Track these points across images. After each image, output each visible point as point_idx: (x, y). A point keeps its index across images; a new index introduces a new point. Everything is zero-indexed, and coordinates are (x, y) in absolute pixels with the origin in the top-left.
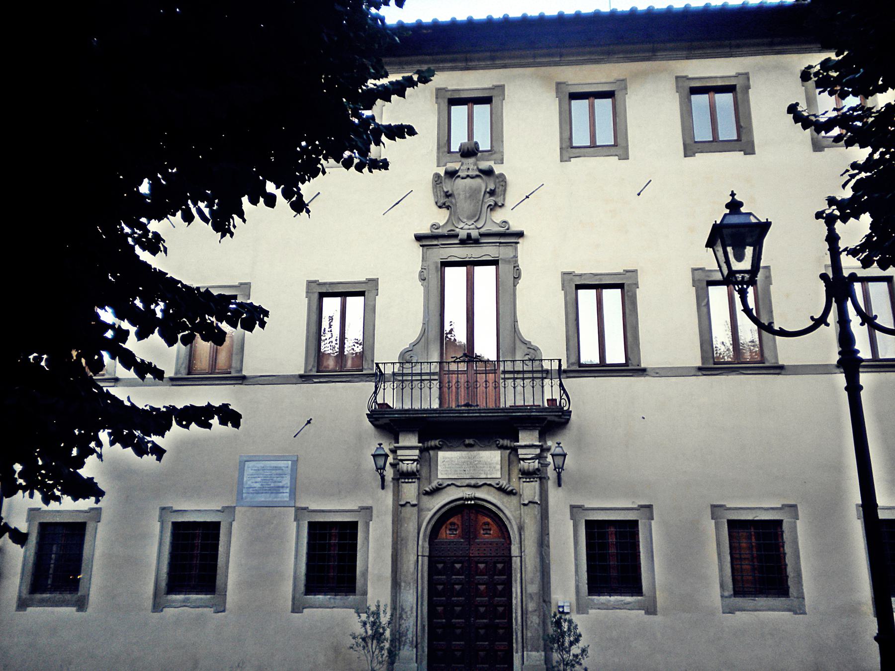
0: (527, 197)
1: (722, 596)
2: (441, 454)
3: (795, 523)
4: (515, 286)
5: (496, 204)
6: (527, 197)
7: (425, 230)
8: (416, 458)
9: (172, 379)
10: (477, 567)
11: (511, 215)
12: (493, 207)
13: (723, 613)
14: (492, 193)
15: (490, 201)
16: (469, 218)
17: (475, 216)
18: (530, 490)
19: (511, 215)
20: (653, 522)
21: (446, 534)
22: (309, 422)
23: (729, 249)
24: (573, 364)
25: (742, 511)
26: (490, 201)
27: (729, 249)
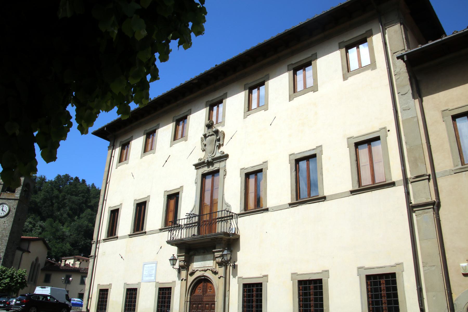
4: (224, 179)
5: (220, 144)
7: (197, 162)
9: (104, 240)
10: (205, 306)
11: (225, 149)
12: (219, 147)
15: (217, 143)
16: (210, 153)
18: (221, 271)
19: (225, 149)
21: (199, 292)
24: (242, 211)
26: (217, 143)
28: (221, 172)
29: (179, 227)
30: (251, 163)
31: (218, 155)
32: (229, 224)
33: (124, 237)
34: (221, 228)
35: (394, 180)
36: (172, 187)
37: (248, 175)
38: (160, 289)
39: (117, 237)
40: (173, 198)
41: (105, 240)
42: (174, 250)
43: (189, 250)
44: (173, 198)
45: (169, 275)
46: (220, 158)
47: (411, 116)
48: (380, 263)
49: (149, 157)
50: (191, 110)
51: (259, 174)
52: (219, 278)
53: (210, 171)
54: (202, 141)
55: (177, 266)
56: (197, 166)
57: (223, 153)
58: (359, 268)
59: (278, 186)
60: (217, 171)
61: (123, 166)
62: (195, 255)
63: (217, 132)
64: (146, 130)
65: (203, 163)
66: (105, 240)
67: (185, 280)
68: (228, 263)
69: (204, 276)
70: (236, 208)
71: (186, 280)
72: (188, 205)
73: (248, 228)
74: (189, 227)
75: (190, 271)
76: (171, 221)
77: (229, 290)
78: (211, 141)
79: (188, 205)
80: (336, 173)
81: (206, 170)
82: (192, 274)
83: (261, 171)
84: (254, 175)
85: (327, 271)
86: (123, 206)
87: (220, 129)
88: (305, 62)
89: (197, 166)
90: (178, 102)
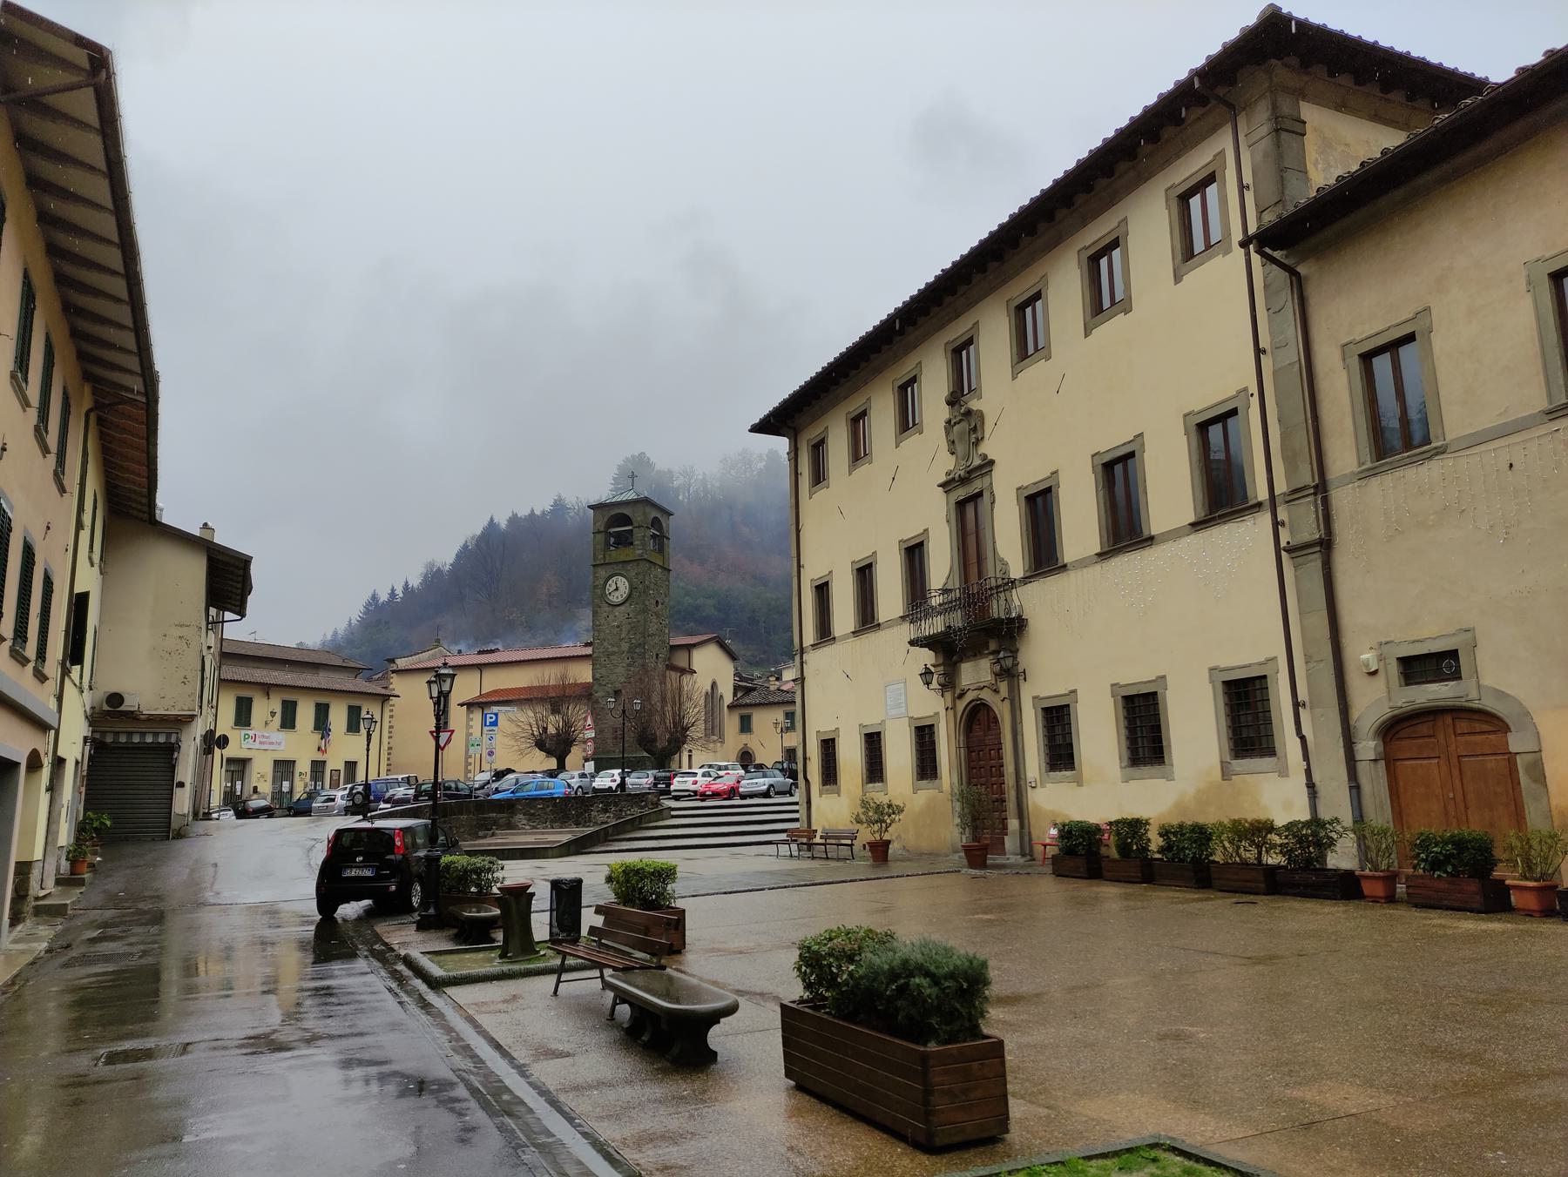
7: (943, 479)
12: (978, 442)
19: (988, 448)
28: (986, 495)
30: (1032, 476)
31: (977, 462)
32: (1002, 602)
33: (845, 637)
35: (1013, 576)
36: (911, 532)
37: (1367, 358)
38: (867, 735)
40: (914, 554)
42: (927, 657)
43: (949, 651)
44: (914, 554)
45: (931, 704)
46: (980, 467)
48: (1242, 657)
49: (864, 470)
50: (1125, 220)
51: (1405, 352)
54: (947, 434)
55: (935, 685)
56: (947, 486)
58: (1211, 669)
59: (1080, 524)
60: (980, 494)
61: (822, 494)
62: (961, 661)
63: (969, 413)
68: (1010, 674)
70: (1017, 570)
72: (940, 568)
73: (1037, 602)
75: (958, 692)
78: (961, 434)
79: (940, 568)
80: (1170, 491)
81: (961, 493)
82: (961, 696)
83: (1132, 455)
84: (1040, 506)
85: (1164, 677)
86: (1063, 479)
87: (974, 405)
88: (1107, 241)
89: (947, 486)
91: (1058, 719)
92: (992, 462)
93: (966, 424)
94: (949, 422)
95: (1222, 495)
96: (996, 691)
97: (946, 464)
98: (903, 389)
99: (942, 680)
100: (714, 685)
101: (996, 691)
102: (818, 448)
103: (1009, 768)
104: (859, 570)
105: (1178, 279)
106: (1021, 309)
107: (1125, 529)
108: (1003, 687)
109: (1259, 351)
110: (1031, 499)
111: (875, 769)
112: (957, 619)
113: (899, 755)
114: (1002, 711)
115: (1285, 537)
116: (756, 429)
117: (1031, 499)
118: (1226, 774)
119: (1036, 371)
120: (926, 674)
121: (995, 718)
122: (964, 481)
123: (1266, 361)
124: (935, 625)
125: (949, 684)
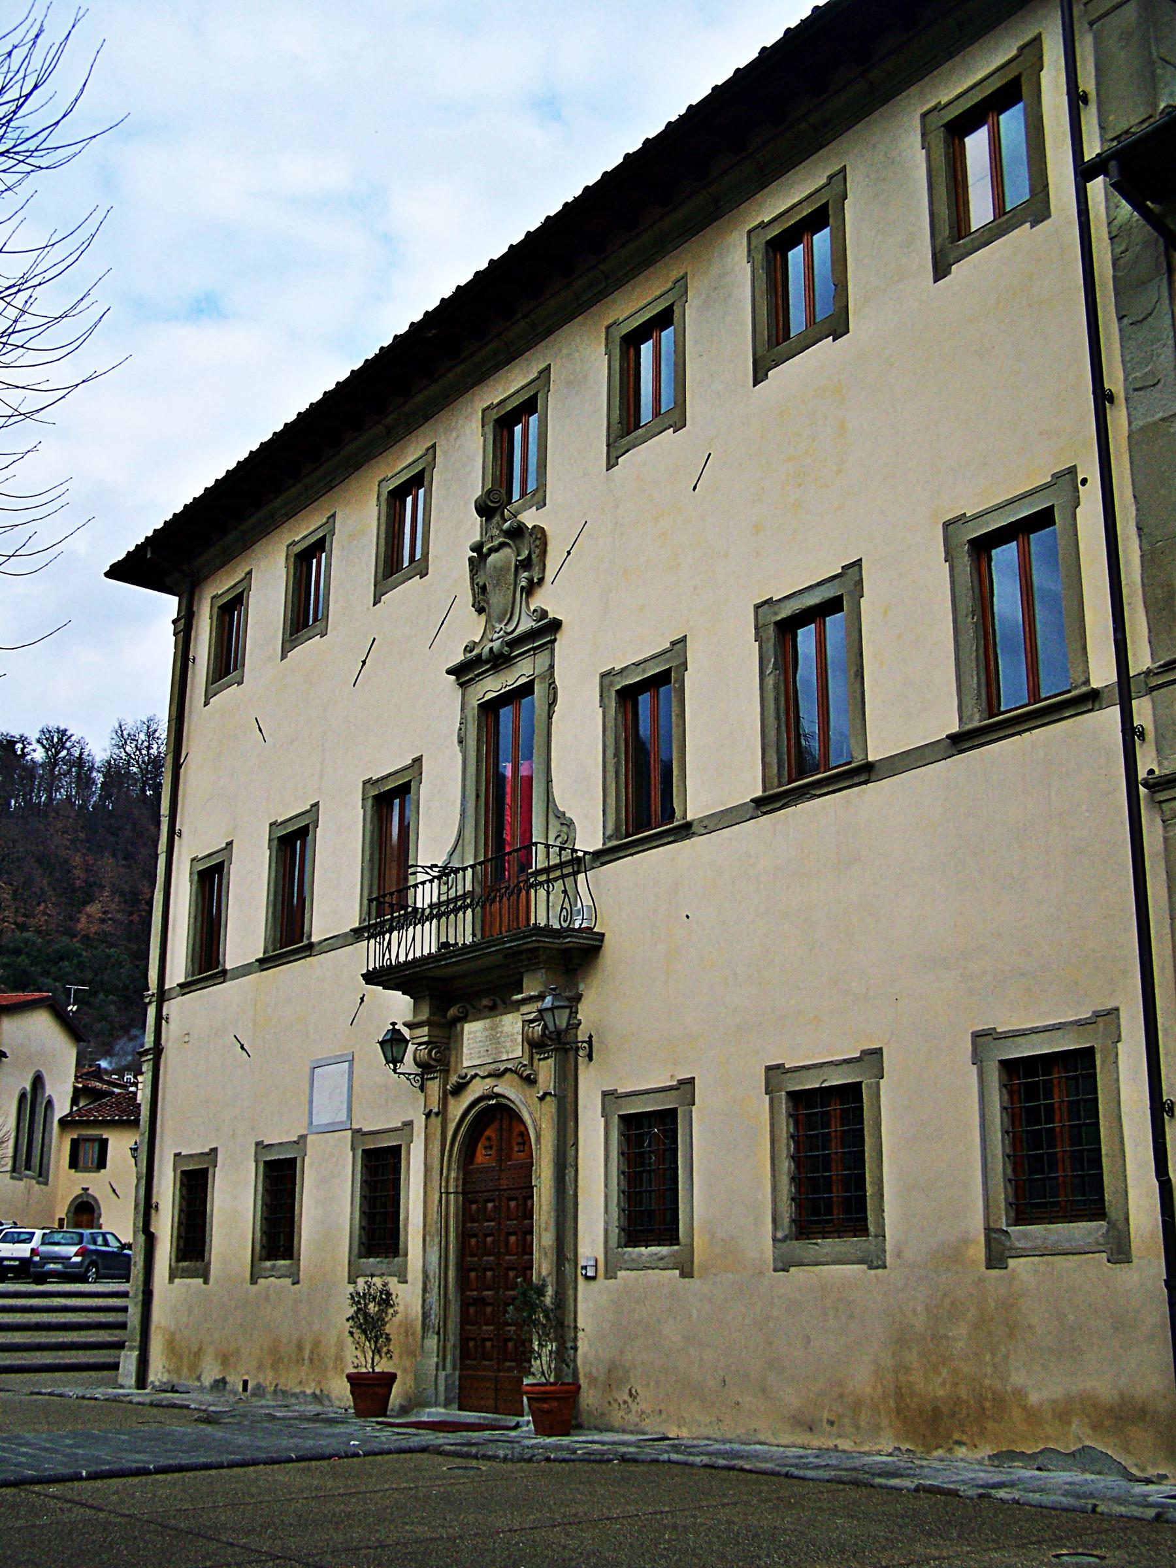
0: (242, 1047)
1: (775, 1239)
2: (467, 1027)
3: (878, 1084)
6: (242, 1047)
7: (459, 658)
8: (426, 1039)
9: (181, 986)
12: (531, 588)
13: (775, 1270)
14: (526, 564)
17: (505, 615)
20: (694, 1108)
21: (481, 1156)
22: (362, 999)
23: (17, 1263)
24: (610, 838)
25: (804, 1073)
27: (17, 1263)
29: (416, 917)
30: (634, 648)
33: (244, 971)
34: (544, 909)
39: (224, 972)
40: (390, 801)
41: (186, 987)
42: (397, 1006)
43: (447, 991)
44: (390, 801)
45: (394, 1103)
46: (531, 635)
47: (1160, 415)
48: (1040, 1016)
49: (310, 648)
52: (542, 1099)
53: (503, 731)
55: (408, 1064)
57: (545, 613)
59: (722, 744)
61: (229, 695)
62: (464, 1018)
63: (517, 533)
64: (294, 543)
65: (478, 660)
66: (186, 987)
67: (437, 1114)
68: (560, 1044)
69: (498, 1095)
70: (590, 837)
71: (442, 1113)
72: (440, 830)
73: (626, 900)
74: (447, 914)
75: (454, 1079)
76: (387, 906)
77: (576, 1144)
80: (908, 679)
81: (491, 686)
82: (459, 1089)
84: (645, 704)
90: (389, 420)
91: (652, 1143)
92: (556, 625)
93: (512, 552)
94: (477, 548)
95: (1009, 692)
96: (530, 1081)
97: (468, 630)
98: (397, 496)
99: (423, 1053)
100: (38, 1081)
101: (530, 1081)
102: (231, 611)
103: (544, 1238)
104: (281, 839)
105: (941, 270)
106: (632, 341)
107: (807, 761)
108: (546, 1071)
109: (1102, 398)
110: (628, 697)
111: (278, 1234)
112: (463, 930)
113: (328, 1206)
114: (539, 1120)
115: (1147, 762)
116: (118, 572)
117: (628, 697)
118: (997, 1254)
119: (655, 453)
120: (393, 1044)
121: (525, 1134)
122: (499, 661)
123: (1118, 420)
124: (418, 942)
125: (438, 1063)
